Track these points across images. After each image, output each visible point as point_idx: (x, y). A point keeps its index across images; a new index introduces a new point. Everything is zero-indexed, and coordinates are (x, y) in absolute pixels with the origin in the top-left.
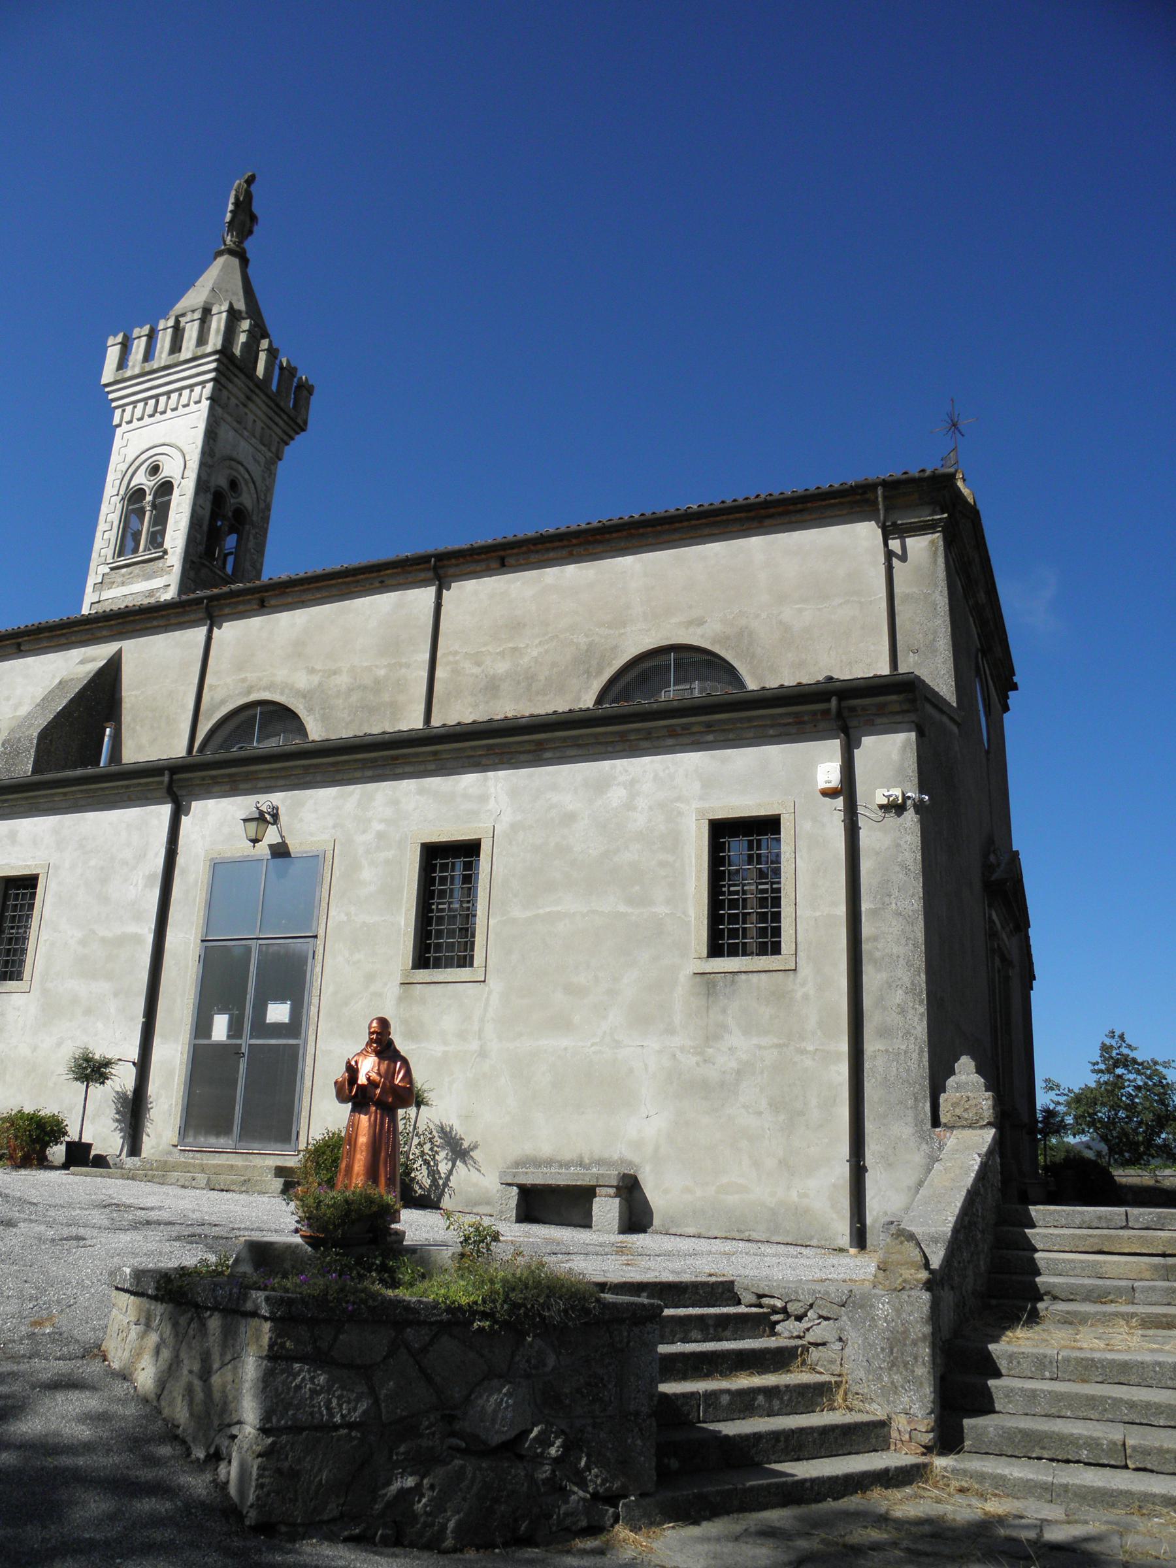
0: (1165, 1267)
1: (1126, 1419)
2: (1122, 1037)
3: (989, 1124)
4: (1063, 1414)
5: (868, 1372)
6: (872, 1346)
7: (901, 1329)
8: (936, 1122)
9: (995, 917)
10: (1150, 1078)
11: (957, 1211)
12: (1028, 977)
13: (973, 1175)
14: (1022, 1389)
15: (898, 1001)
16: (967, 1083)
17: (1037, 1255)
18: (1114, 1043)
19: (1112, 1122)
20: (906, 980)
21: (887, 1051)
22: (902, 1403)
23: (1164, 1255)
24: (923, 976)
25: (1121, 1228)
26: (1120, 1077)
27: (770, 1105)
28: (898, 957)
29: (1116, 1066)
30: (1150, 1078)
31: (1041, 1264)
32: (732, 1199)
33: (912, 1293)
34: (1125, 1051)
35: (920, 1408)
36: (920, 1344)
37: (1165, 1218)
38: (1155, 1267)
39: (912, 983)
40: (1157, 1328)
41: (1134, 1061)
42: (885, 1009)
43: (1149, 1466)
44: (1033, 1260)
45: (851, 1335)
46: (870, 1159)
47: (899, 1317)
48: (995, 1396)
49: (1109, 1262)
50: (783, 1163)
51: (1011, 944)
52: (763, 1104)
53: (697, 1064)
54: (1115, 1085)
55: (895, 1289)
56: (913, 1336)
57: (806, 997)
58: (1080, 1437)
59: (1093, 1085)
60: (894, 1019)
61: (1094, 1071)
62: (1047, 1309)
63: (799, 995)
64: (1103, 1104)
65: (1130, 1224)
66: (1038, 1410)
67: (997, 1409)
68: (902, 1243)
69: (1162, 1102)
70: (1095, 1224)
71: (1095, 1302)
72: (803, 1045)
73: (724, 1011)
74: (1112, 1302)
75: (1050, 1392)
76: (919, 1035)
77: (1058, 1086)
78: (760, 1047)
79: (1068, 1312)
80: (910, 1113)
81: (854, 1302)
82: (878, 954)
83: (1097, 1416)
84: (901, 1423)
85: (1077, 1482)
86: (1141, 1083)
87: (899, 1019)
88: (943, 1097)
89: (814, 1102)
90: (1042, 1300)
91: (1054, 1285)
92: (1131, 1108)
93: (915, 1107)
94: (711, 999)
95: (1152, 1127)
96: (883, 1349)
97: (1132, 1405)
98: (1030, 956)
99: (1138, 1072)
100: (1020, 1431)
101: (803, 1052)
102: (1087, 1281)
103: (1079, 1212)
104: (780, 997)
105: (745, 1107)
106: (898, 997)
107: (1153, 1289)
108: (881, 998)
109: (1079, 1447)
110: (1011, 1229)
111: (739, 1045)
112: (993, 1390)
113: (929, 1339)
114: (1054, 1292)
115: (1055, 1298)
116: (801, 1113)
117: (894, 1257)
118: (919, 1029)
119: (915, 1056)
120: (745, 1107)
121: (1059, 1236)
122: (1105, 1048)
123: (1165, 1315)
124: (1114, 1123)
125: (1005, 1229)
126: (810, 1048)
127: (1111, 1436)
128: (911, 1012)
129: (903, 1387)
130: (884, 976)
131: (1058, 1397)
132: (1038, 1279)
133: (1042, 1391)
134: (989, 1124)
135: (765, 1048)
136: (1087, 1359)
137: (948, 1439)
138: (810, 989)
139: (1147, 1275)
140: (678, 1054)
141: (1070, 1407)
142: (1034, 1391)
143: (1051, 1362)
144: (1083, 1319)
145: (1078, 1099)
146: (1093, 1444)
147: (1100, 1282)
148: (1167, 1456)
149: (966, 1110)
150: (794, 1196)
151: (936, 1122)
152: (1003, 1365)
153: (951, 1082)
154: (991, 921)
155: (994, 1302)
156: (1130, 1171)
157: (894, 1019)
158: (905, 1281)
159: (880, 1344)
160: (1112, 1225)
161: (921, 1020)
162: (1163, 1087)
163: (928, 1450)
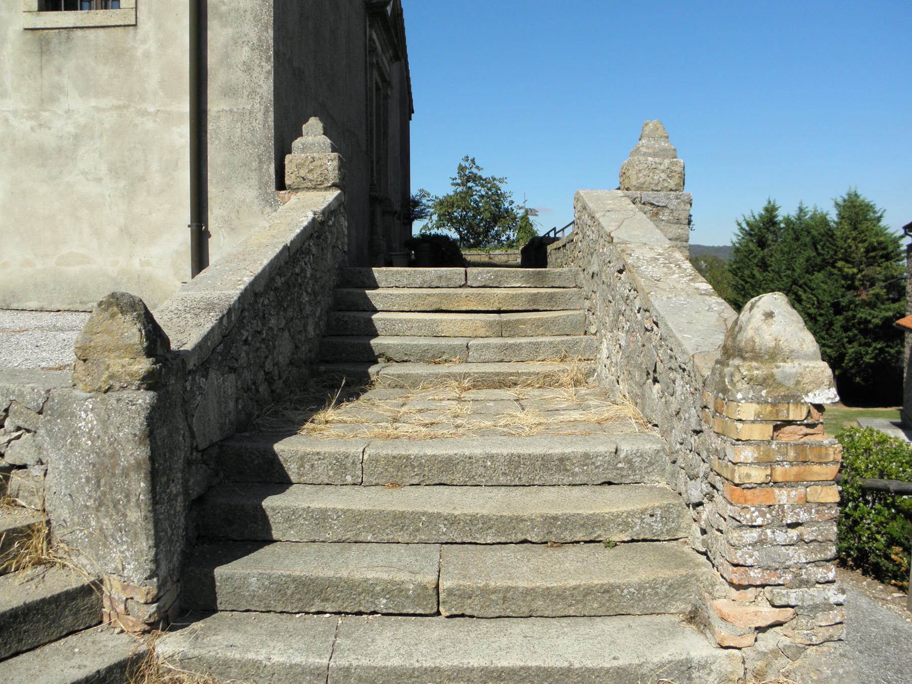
0: (501, 324)
1: (444, 539)
2: (473, 161)
3: (334, 185)
4: (361, 539)
5: (72, 511)
6: (75, 473)
7: (109, 451)
8: (281, 185)
9: (375, 36)
10: (489, 189)
11: (259, 269)
12: (407, 110)
13: (298, 231)
14: (307, 510)
15: (244, 58)
16: (314, 146)
17: (375, 317)
18: (467, 165)
19: (464, 218)
20: (253, 36)
21: (231, 111)
22: (113, 560)
23: (499, 312)
24: (271, 32)
25: (460, 287)
26: (470, 188)
27: (110, 170)
28: (245, 11)
29: (468, 181)
30: (489, 189)
31: (378, 325)
32: (74, 270)
33: (125, 394)
34: (474, 170)
35: (136, 570)
36: (133, 475)
37: (502, 276)
38: (490, 324)
39: (259, 40)
40: (489, 387)
41: (480, 178)
42: (230, 67)
43: (468, 612)
44: (371, 320)
45: (53, 457)
46: (213, 223)
47: (106, 433)
48: (271, 520)
49: (445, 321)
50: (125, 231)
51: (392, 70)
52: (103, 169)
53: (32, 129)
54: (466, 193)
55: (98, 390)
56: (123, 463)
57: (147, 55)
58: (378, 581)
59: (452, 193)
60: (238, 77)
61: (453, 184)
62: (378, 373)
63: (139, 52)
64: (458, 207)
65: (469, 283)
66: (329, 535)
67: (275, 537)
68: (113, 316)
69: (497, 206)
70: (435, 284)
71: (429, 362)
72: (144, 106)
73: (59, 71)
74: (446, 361)
75: (344, 512)
76: (265, 94)
77: (429, 194)
78: (98, 109)
79: (399, 376)
80: (254, 176)
81: (51, 408)
82: (224, 8)
83: (406, 538)
84: (113, 589)
85: (364, 662)
86: (484, 193)
87: (244, 77)
88: (288, 158)
89: (155, 166)
90: (377, 362)
91: (388, 347)
92: (477, 209)
93: (260, 169)
94: (45, 58)
95: (489, 222)
96: (88, 480)
97: (452, 521)
98: (410, 94)
99: (483, 186)
100: (294, 580)
101: (143, 113)
102: (423, 341)
103: (421, 273)
104: (120, 55)
105: (84, 173)
106: (245, 53)
107: (487, 347)
108: (227, 56)
109: (376, 596)
110: (351, 290)
111: (77, 107)
112: (269, 513)
113: (147, 467)
114: (388, 354)
115: (389, 360)
116: (142, 179)
117: (98, 340)
118: (265, 87)
119: (260, 116)
120: (84, 173)
121: (399, 296)
122: (462, 169)
123: (498, 374)
124: (465, 220)
125: (345, 290)
126: (152, 109)
127: (419, 578)
128: (258, 69)
129: (113, 536)
130: (229, 31)
131: (355, 517)
132: (373, 342)
133: (335, 510)
134: (334, 185)
135: (104, 110)
136: (401, 457)
137: (186, 599)
138: (151, 45)
139: (482, 332)
140: (11, 117)
141: (370, 528)
142: (324, 511)
143: (353, 462)
144: (415, 382)
145: (441, 203)
146: (394, 590)
147: (434, 342)
148: (493, 597)
149: (311, 171)
150: (136, 264)
151: (281, 185)
152: (292, 471)
153: (297, 143)
154: (371, 40)
155: (322, 368)
156: (473, 252)
157: (238, 77)
158: (111, 377)
159: (86, 472)
160: (452, 284)
161: (267, 78)
162: (498, 195)
163: (152, 627)
